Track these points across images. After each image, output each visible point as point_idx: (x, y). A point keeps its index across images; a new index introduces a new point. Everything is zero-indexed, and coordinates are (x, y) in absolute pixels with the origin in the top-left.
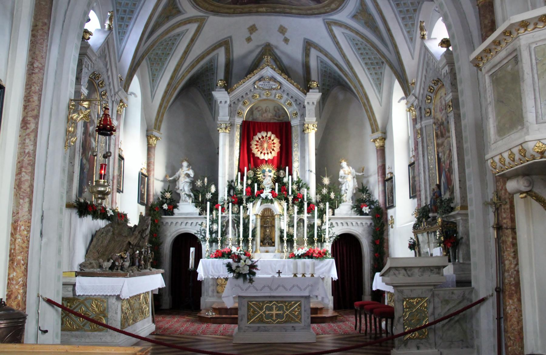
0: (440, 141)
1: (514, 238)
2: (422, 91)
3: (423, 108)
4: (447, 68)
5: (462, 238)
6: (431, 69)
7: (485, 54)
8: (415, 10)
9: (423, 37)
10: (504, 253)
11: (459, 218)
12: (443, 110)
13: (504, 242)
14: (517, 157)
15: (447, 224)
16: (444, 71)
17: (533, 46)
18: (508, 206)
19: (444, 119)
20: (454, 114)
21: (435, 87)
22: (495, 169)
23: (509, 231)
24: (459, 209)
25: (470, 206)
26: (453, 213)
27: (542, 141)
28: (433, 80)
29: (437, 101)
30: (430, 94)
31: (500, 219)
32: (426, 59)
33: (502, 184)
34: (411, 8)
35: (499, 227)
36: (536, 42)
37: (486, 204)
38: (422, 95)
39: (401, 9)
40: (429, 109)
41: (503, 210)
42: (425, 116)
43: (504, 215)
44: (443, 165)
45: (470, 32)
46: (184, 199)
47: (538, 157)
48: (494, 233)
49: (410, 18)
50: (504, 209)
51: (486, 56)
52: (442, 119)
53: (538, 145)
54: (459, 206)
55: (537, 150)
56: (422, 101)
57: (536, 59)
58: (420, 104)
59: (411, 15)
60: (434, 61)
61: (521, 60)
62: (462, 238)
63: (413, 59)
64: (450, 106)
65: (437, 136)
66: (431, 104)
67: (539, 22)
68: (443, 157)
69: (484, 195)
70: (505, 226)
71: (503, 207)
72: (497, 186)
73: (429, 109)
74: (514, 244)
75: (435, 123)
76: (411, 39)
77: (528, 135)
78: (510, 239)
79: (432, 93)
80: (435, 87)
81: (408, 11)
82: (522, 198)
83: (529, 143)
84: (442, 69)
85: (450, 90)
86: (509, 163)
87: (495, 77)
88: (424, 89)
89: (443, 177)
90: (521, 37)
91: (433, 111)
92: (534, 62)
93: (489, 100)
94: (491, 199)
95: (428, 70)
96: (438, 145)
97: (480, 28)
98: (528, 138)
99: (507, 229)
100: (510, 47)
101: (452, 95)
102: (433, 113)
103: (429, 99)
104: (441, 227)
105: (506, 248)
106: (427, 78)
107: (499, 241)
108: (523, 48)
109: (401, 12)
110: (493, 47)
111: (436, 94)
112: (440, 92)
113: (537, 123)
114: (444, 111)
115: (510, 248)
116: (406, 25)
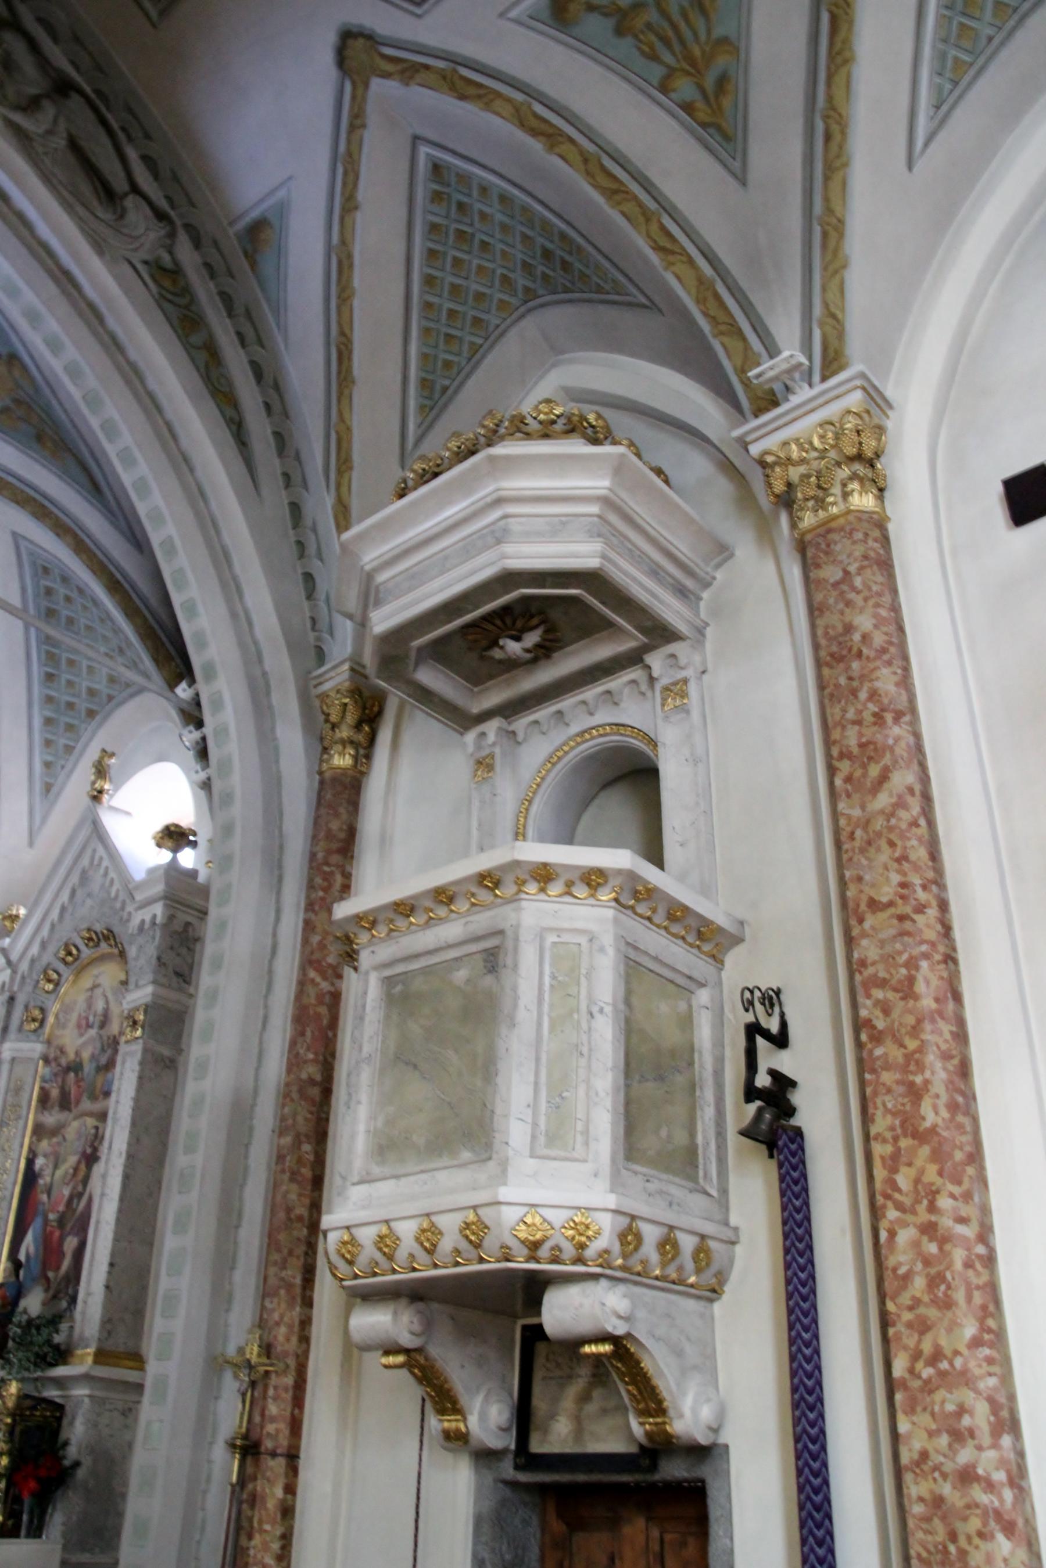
0: (50, 1119)
1: (290, 1489)
2: (35, 950)
3: (21, 1000)
4: (158, 910)
5: (77, 1464)
6: (89, 895)
7: (392, 915)
8: (91, 714)
9: (97, 796)
10: (250, 1537)
11: (81, 1392)
12: (89, 1026)
13: (253, 1500)
14: (446, 1245)
15: (34, 1408)
16: (146, 915)
17: (551, 938)
18: (289, 1380)
19: (86, 1055)
20: (145, 1051)
21: (86, 952)
22: (351, 1263)
23: (277, 1466)
24: (90, 1360)
25: (159, 1359)
26: (60, 1371)
27: (540, 1210)
28: (89, 930)
29: (74, 994)
30: (61, 967)
31: (257, 1419)
32: (85, 862)
33: (283, 1305)
34: (83, 705)
35: (249, 1448)
36: (559, 931)
37: (216, 1364)
38: (33, 961)
39: (53, 694)
40: (42, 1010)
41: (271, 1392)
42: (20, 1029)
43: (273, 1409)
44: (44, 1197)
45: (281, 835)
46: (960, 1503)
47: (521, 1252)
48: (225, 1467)
49: (70, 727)
50: (276, 1388)
51: (391, 921)
52: (77, 1053)
53: (529, 1220)
54: (91, 1350)
55: (522, 1235)
56: (23, 978)
57: (553, 977)
58: (15, 988)
59: (75, 722)
60: (112, 874)
61: (516, 967)
62: (77, 1464)
63: (31, 844)
64: (135, 1023)
65: (44, 1100)
66: (53, 996)
67: (578, 882)
68: (47, 1172)
69: (215, 1331)
70: (268, 1444)
71: (274, 1380)
72: (263, 1308)
73: (42, 1010)
74: (287, 1512)
75: (46, 1060)
76: (48, 788)
77: (505, 1184)
78: (279, 1492)
79: (66, 963)
80: (86, 952)
81: (70, 706)
82: (386, 1367)
83: (504, 1208)
84: (140, 908)
85: (150, 977)
86: (412, 1256)
87: (399, 988)
88: (44, 945)
89: (29, 1239)
90: (524, 904)
91: (51, 1019)
92: (547, 980)
93: (367, 1049)
94: (241, 1351)
95: (79, 893)
96: (39, 1131)
97: (310, 833)
98: (504, 1193)
99: (274, 1454)
100: (482, 921)
101: (153, 994)
102: (47, 1029)
103: (49, 981)
104: (13, 1415)
105: (260, 1522)
106: (67, 916)
107: (244, 1495)
108: (525, 936)
109: (49, 700)
110: (428, 903)
111: (78, 973)
112: (95, 971)
113: (532, 1157)
114: (92, 1032)
115: (273, 1523)
116: (48, 743)
